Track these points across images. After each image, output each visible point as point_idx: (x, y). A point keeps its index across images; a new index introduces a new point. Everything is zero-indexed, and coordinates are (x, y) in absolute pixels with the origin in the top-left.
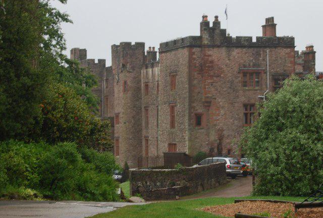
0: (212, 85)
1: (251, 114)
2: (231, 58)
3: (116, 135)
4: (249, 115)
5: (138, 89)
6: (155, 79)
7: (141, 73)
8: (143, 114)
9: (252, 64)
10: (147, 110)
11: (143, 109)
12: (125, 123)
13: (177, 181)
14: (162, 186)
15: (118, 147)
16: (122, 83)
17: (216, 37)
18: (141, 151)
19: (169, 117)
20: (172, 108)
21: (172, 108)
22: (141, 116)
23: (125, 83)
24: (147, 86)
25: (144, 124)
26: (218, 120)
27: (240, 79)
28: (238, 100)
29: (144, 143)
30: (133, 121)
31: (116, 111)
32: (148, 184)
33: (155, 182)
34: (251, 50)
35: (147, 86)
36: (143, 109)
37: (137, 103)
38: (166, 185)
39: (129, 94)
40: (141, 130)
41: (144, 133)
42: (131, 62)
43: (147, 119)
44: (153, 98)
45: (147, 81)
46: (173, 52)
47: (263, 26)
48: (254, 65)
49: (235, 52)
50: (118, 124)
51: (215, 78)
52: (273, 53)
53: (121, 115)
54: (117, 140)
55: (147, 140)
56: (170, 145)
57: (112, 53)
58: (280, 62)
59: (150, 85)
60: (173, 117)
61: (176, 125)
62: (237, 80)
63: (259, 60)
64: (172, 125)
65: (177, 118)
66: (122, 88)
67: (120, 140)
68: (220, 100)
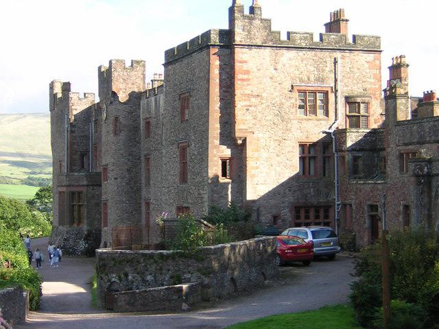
0: (248, 110)
1: (310, 158)
2: (279, 67)
3: (104, 197)
4: (307, 159)
5: (136, 129)
6: (159, 111)
7: (139, 105)
8: (143, 164)
9: (312, 78)
10: (148, 160)
11: (143, 159)
12: (116, 179)
13: (184, 273)
14: (157, 283)
15: (106, 214)
16: (111, 119)
17: (254, 31)
18: (140, 221)
19: (177, 166)
20: (183, 151)
21: (183, 151)
22: (140, 169)
23: (116, 119)
24: (148, 124)
25: (143, 181)
26: (257, 168)
27: (293, 101)
28: (290, 135)
29: (143, 208)
30: (127, 176)
31: (104, 163)
32: (130, 277)
33: (142, 274)
34: (310, 54)
35: (148, 124)
36: (143, 159)
37: (134, 149)
38: (164, 280)
39: (122, 136)
40: (139, 190)
41: (144, 193)
42: (125, 89)
43: (149, 173)
44: (157, 140)
45: (148, 116)
46: (185, 61)
47: (389, 68)
48: (318, 80)
49: (287, 55)
50: (107, 181)
51: (253, 100)
52: (347, 60)
53: (110, 168)
54: (105, 204)
55: (148, 204)
56: (180, 209)
57: (99, 85)
58: (357, 74)
59: (153, 121)
60: (184, 165)
61: (189, 177)
62: (288, 104)
63: (323, 71)
64: (183, 179)
65: (190, 165)
66: (111, 127)
67: (109, 204)
68: (260, 135)
